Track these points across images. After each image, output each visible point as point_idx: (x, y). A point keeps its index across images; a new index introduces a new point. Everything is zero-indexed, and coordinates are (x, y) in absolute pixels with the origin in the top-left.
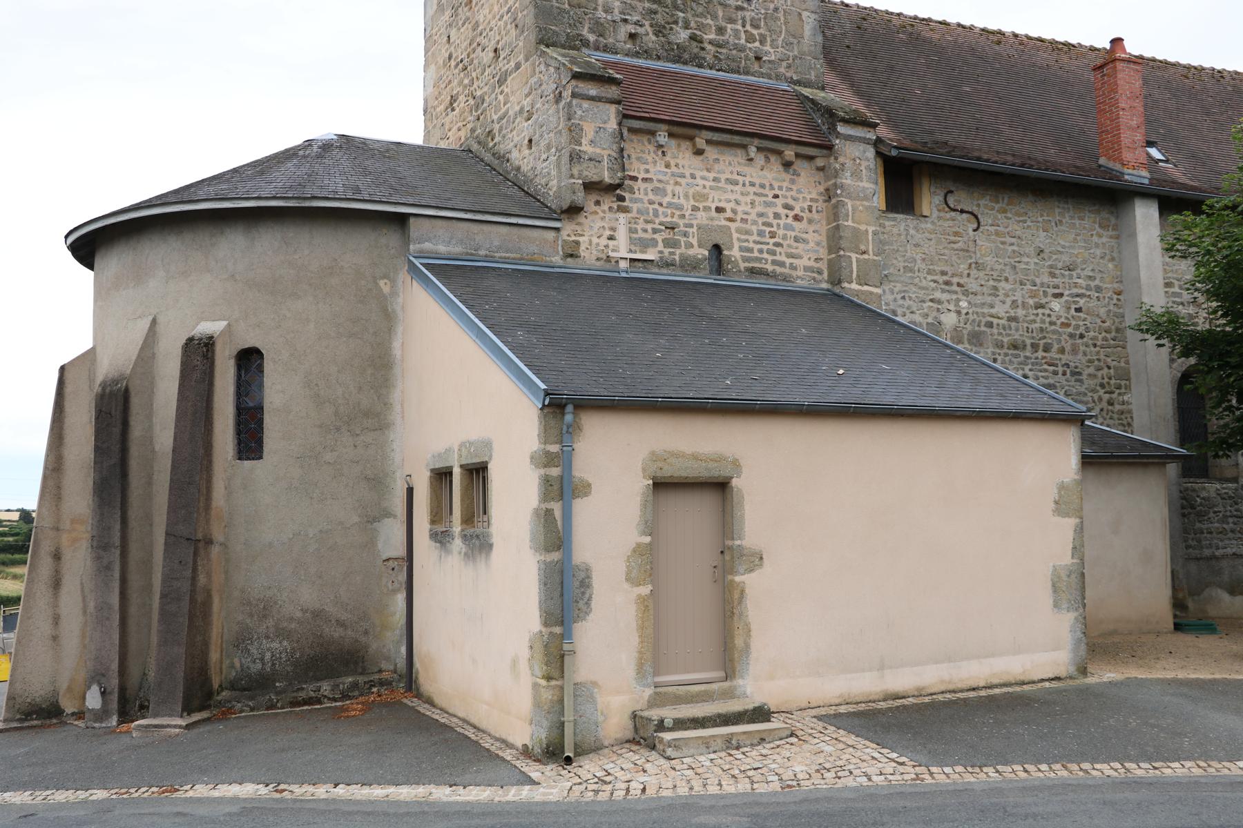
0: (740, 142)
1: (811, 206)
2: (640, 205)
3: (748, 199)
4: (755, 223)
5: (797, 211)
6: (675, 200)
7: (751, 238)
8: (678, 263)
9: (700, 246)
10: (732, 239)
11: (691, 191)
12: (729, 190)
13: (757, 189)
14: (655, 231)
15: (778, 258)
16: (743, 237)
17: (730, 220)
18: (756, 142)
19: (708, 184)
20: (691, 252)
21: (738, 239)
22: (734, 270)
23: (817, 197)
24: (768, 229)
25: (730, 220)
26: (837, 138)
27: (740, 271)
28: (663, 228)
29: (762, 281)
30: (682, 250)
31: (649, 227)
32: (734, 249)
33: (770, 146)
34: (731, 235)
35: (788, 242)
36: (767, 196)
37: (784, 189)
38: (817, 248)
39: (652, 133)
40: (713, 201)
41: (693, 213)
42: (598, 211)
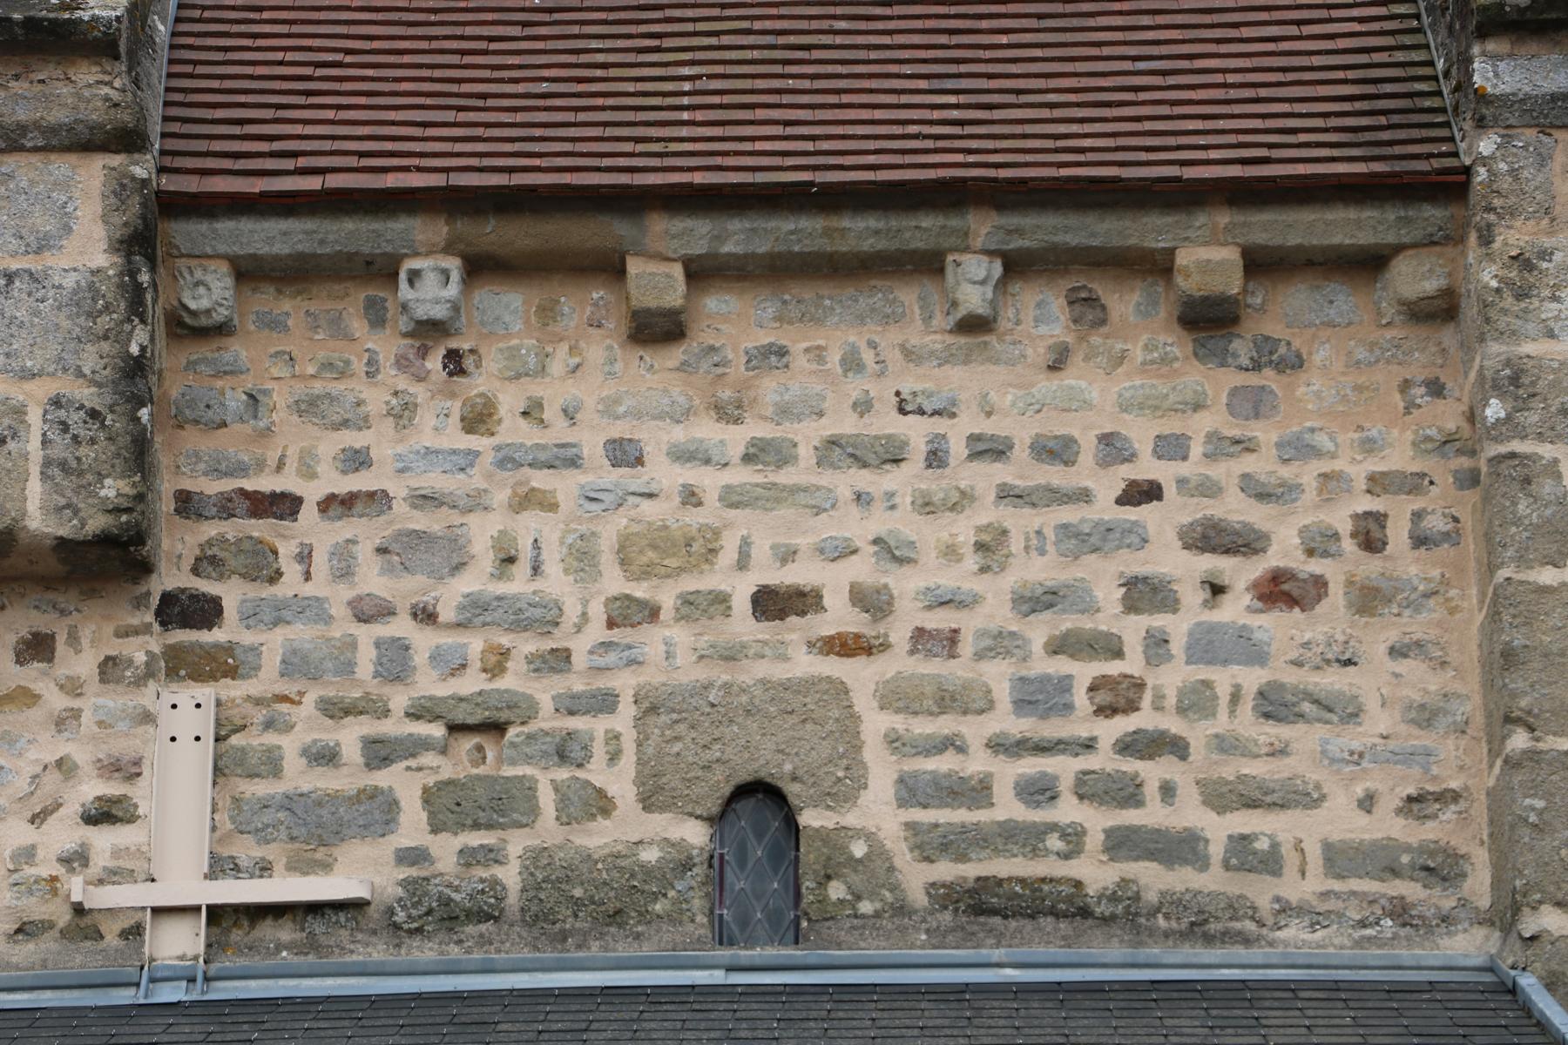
0: (882, 244)
1: (1380, 518)
2: (301, 633)
3: (964, 529)
4: (1000, 644)
5: (1285, 551)
6: (518, 585)
7: (975, 730)
8: (513, 899)
9: (649, 801)
10: (858, 748)
11: (610, 531)
12: (844, 493)
13: (1020, 471)
14: (380, 753)
15: (1151, 815)
16: (924, 727)
17: (845, 646)
18: (983, 226)
19: (710, 481)
20: (598, 837)
21: (895, 742)
22: (866, 907)
23: (1415, 467)
24: (1084, 672)
25: (845, 646)
26: (1481, 124)
27: (901, 909)
28: (437, 731)
29: (1040, 952)
30: (548, 829)
31: (350, 736)
32: (865, 798)
33: (1072, 240)
34: (850, 725)
35: (1221, 722)
36: (1084, 496)
37: (1196, 450)
38: (1423, 739)
39: (929, 265)
40: (743, 563)
41: (616, 635)
42: (38, 687)
